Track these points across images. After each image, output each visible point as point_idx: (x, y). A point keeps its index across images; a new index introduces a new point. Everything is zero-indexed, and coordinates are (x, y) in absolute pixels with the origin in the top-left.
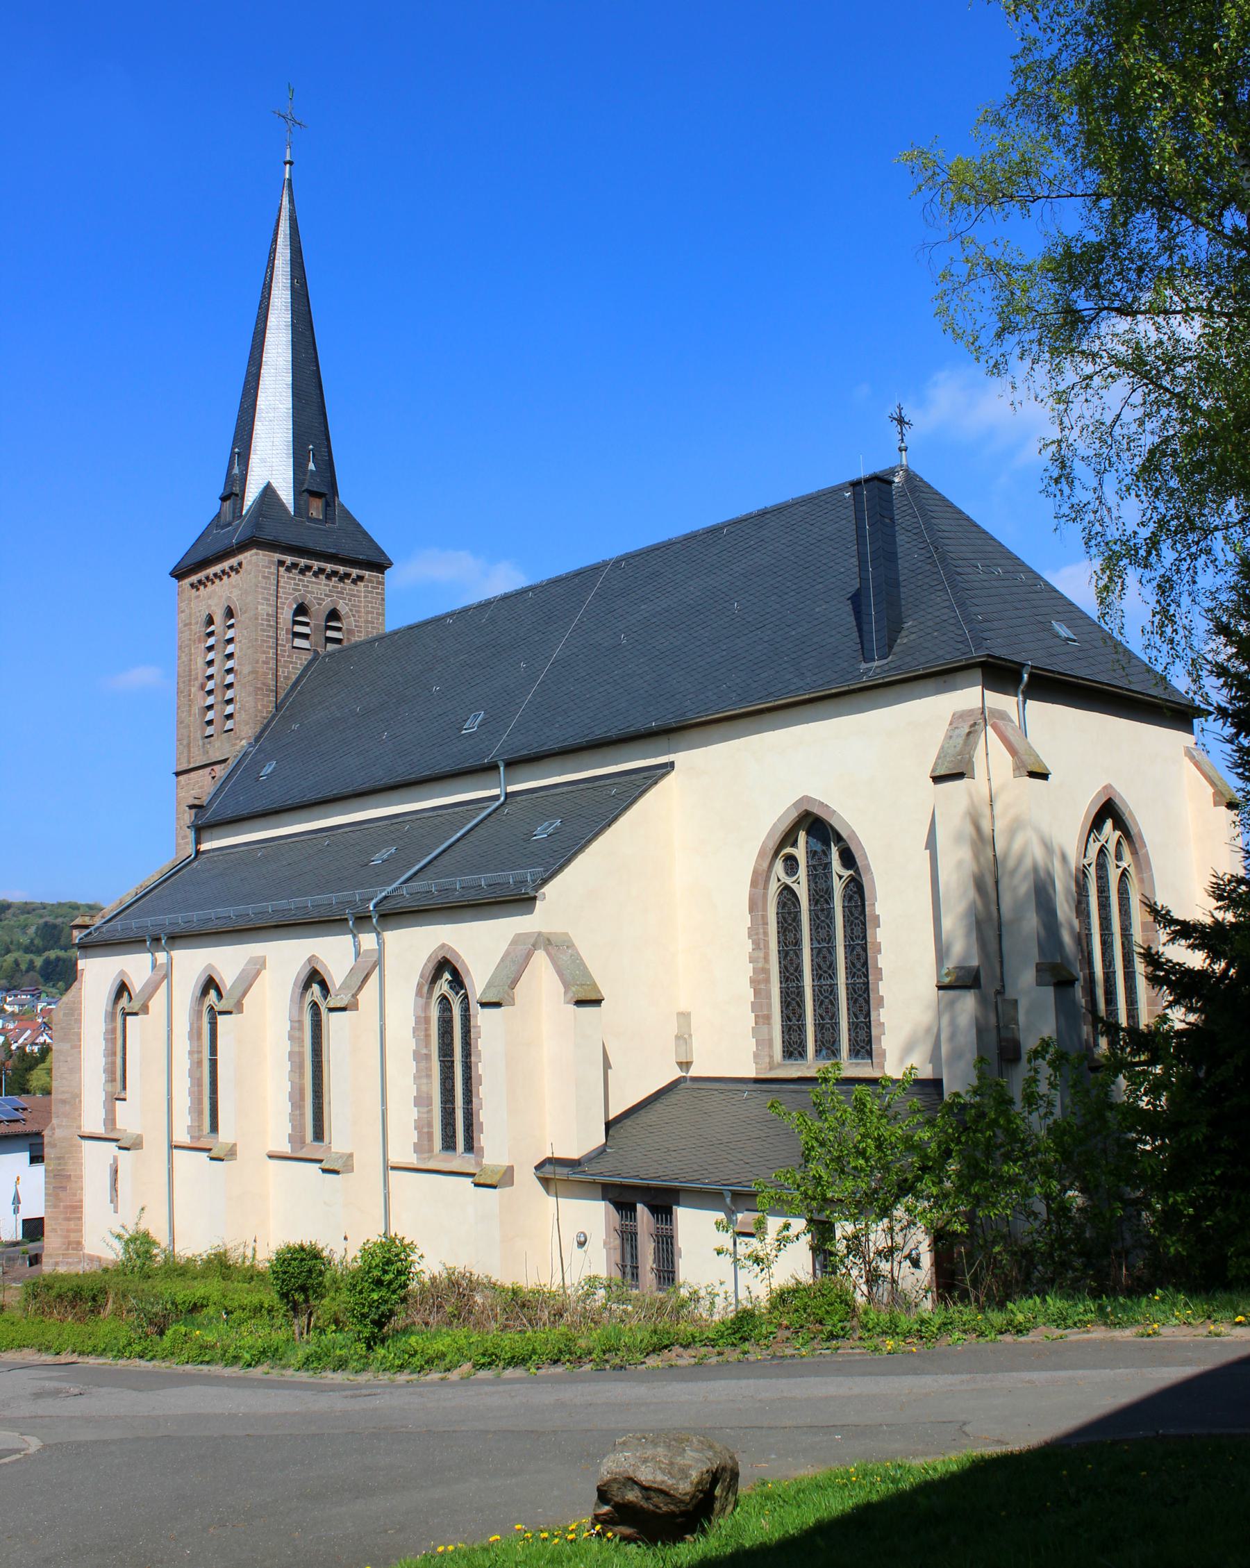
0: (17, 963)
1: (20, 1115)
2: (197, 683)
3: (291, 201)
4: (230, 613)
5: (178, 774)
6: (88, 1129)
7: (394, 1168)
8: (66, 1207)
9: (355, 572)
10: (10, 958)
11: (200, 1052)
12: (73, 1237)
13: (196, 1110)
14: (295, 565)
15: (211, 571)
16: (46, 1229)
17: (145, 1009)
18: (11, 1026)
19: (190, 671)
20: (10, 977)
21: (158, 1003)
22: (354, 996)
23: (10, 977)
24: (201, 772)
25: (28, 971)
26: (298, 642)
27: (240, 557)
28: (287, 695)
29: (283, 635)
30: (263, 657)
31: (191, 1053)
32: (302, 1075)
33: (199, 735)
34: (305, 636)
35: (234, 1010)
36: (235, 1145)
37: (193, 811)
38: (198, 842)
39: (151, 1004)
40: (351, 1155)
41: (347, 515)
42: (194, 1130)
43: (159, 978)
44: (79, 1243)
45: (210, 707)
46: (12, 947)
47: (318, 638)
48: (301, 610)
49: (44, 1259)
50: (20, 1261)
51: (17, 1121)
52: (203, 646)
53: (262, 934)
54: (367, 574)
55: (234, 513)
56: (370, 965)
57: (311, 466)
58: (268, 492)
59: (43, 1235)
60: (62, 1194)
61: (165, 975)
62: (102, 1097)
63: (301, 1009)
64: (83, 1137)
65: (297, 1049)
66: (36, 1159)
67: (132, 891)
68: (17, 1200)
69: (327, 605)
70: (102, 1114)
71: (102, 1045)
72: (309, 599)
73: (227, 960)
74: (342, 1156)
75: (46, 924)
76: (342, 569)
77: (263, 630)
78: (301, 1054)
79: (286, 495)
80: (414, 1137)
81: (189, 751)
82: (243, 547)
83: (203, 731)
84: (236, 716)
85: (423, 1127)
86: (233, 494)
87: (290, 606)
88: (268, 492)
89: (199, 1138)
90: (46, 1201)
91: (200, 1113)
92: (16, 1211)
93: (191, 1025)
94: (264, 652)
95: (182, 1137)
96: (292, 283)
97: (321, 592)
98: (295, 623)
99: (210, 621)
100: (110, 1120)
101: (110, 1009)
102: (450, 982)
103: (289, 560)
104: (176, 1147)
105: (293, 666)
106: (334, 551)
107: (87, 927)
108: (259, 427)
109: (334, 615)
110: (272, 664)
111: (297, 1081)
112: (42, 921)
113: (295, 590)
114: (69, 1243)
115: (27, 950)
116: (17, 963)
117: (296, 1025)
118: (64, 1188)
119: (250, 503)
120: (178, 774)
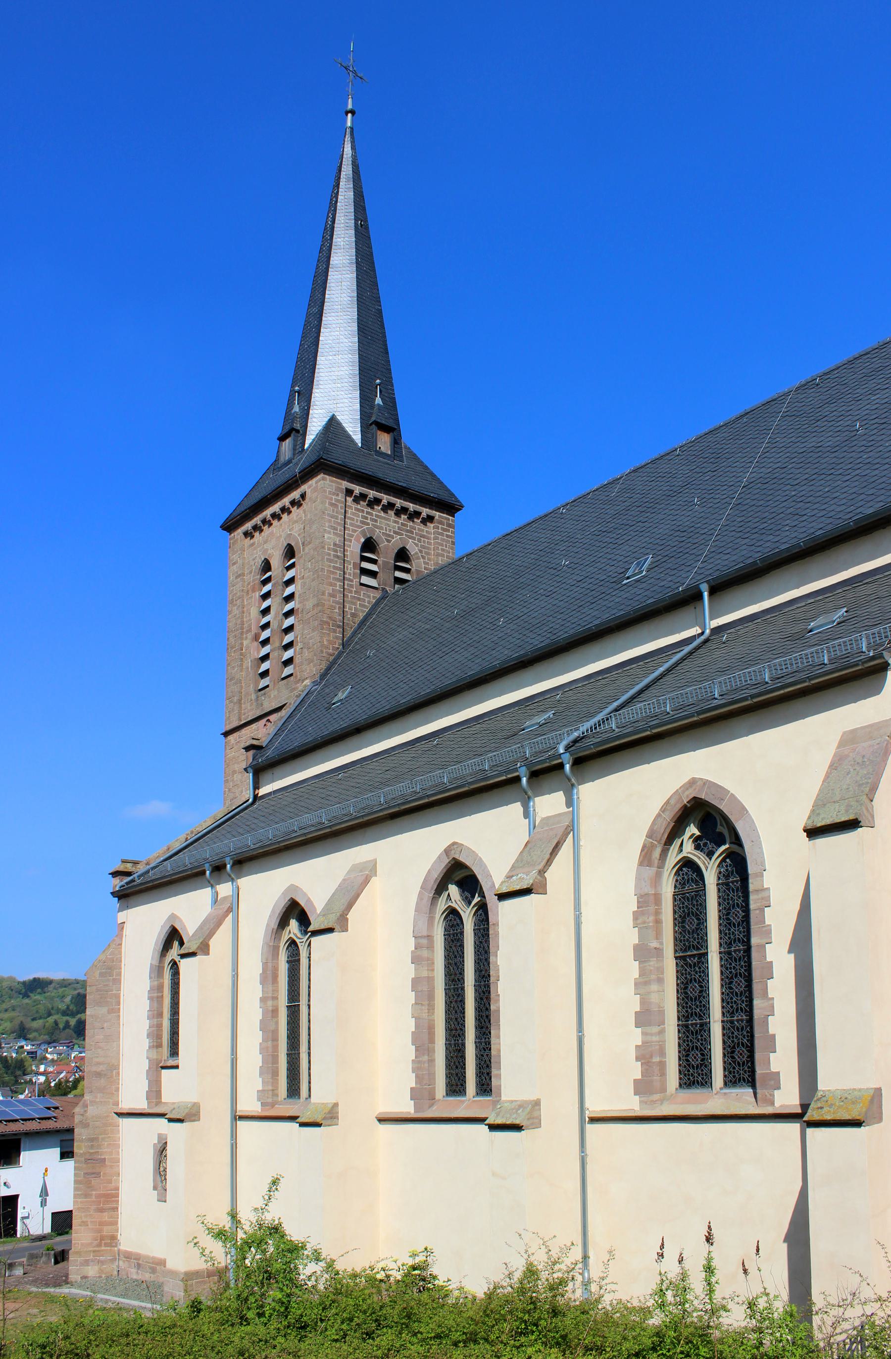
0: (56, 1023)
1: (51, 1113)
2: (250, 636)
3: (353, 142)
4: (290, 552)
5: (226, 734)
6: (126, 1105)
7: (593, 1120)
8: (99, 1196)
9: (425, 511)
10: (51, 1020)
11: (275, 998)
12: (107, 1231)
13: (269, 1069)
14: (363, 496)
15: (267, 513)
16: (75, 1222)
17: (204, 948)
18: (51, 1069)
19: (242, 623)
20: (51, 1034)
21: (220, 942)
22: (542, 872)
23: (51, 1034)
24: (254, 726)
25: (64, 1028)
26: (365, 580)
27: (304, 488)
28: (355, 633)
29: (350, 570)
30: (330, 589)
31: (263, 1000)
32: (431, 1008)
33: (252, 688)
34: (373, 574)
35: (337, 927)
36: (336, 1105)
37: (251, 753)
38: (256, 786)
39: (212, 943)
40: (537, 1103)
41: (414, 457)
42: (266, 1096)
43: (221, 912)
44: (114, 1238)
45: (265, 658)
46: (53, 1012)
47: (386, 577)
48: (369, 545)
49: (72, 1257)
50: (44, 1259)
51: (49, 1118)
52: (257, 595)
53: (370, 831)
54: (437, 514)
55: (294, 449)
56: (560, 832)
57: (378, 401)
58: (333, 425)
59: (71, 1227)
60: (94, 1182)
61: (230, 909)
62: (146, 1065)
63: (431, 919)
64: (120, 1115)
65: (425, 974)
66: (66, 1154)
67: (182, 837)
68: (44, 1192)
69: (396, 543)
70: (144, 1086)
71: (145, 1005)
72: (378, 535)
73: (315, 878)
74: (522, 1105)
75: (79, 994)
76: (412, 507)
77: (330, 561)
78: (430, 980)
79: (353, 429)
80: (636, 1071)
81: (241, 707)
82: (307, 474)
83: (257, 684)
84: (297, 660)
85: (647, 1056)
86: (293, 430)
87: (358, 540)
88: (333, 425)
89: (273, 1105)
90: (76, 1189)
91: (275, 1073)
92: (44, 1203)
93: (265, 965)
94: (331, 584)
95: (249, 1104)
96: (356, 224)
97: (389, 529)
98: (364, 559)
99: (267, 566)
100: (155, 1091)
101: (156, 962)
102: (695, 841)
103: (357, 489)
104: (242, 1118)
105: (361, 603)
106: (404, 485)
107: (128, 874)
108: (323, 361)
109: (402, 555)
110: (339, 597)
111: (425, 1015)
112: (76, 992)
113: (362, 522)
114: (102, 1238)
115: (65, 1013)
116: (56, 1023)
117: (423, 941)
118: (97, 1175)
119: (313, 437)
120: (226, 734)
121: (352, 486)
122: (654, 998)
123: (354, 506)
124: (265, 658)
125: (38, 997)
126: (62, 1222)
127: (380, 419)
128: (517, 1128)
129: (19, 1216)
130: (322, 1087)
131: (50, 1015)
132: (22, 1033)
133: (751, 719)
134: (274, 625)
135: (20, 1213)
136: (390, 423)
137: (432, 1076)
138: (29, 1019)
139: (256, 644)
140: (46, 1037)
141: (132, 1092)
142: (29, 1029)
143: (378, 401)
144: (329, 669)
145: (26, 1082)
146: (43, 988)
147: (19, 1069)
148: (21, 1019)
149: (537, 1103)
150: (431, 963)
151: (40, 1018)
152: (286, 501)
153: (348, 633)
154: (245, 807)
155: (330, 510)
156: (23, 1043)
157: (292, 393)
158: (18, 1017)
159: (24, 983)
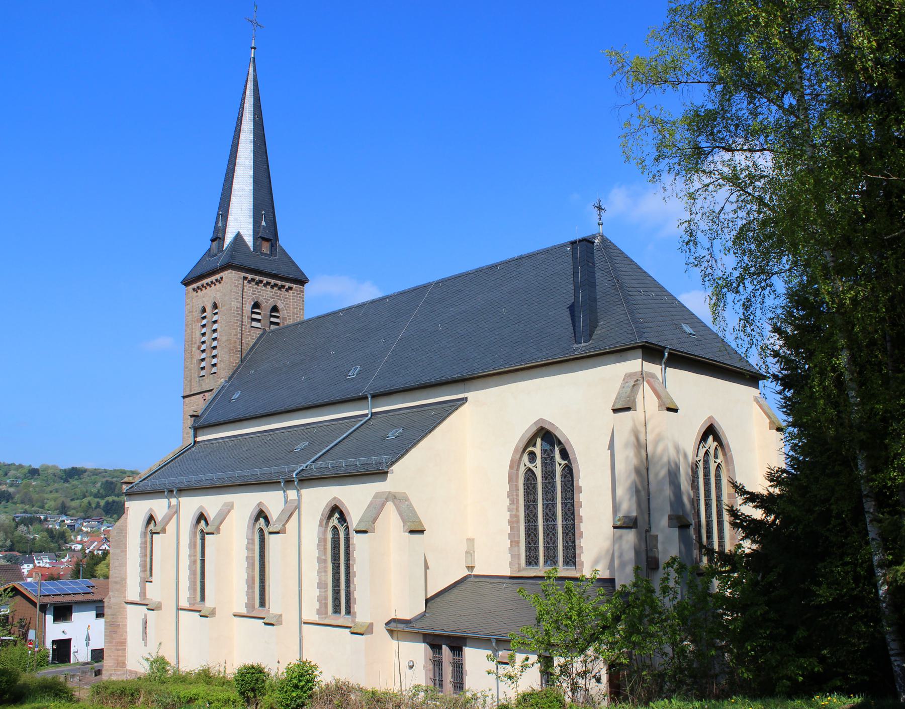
0: (89, 503)
1: (91, 590)
2: (196, 346)
3: (255, 70)
4: (215, 306)
5: (184, 397)
6: (130, 598)
7: (305, 623)
9: (287, 285)
10: (86, 500)
13: (192, 588)
14: (253, 280)
15: (205, 282)
17: (164, 531)
18: (86, 539)
20: (86, 511)
21: (171, 527)
22: (284, 525)
23: (86, 511)
26: (254, 324)
27: (222, 274)
29: (246, 320)
32: (253, 569)
33: (196, 375)
34: (258, 321)
38: (195, 436)
40: (281, 615)
41: (284, 252)
42: (191, 600)
44: (124, 663)
45: (203, 360)
48: (256, 305)
52: (200, 325)
54: (294, 286)
57: (263, 223)
58: (238, 237)
63: (253, 532)
64: (127, 603)
66: (99, 615)
67: (157, 463)
68: (88, 639)
72: (261, 300)
75: (107, 481)
76: (280, 283)
78: (253, 558)
79: (249, 239)
82: (223, 268)
83: (199, 373)
85: (322, 600)
86: (218, 237)
88: (238, 237)
89: (194, 604)
92: (88, 645)
95: (184, 603)
97: (267, 295)
98: (253, 313)
99: (204, 310)
100: (143, 593)
103: (250, 276)
105: (251, 337)
107: (131, 483)
108: (234, 200)
109: (275, 309)
110: (239, 336)
112: (104, 480)
114: (118, 663)
115: (96, 496)
117: (251, 541)
120: (184, 397)
121: (246, 275)
122: (323, 578)
123: (248, 285)
124: (203, 360)
125: (75, 482)
126: (98, 655)
127: (267, 232)
128: (272, 625)
129: (72, 650)
130: (209, 603)
131: (85, 497)
132: (64, 510)
133: (351, 479)
134: (208, 343)
135: (73, 649)
136: (270, 237)
137: (253, 599)
138: (69, 499)
139: (199, 351)
140: (82, 514)
141: (133, 594)
142: (69, 508)
143: (263, 223)
144: (233, 374)
145: (67, 549)
146: (79, 475)
147: (62, 538)
148: (63, 499)
149: (281, 615)
150: (253, 550)
151: (78, 499)
152: (213, 278)
153: (244, 354)
154: (188, 448)
155: (235, 289)
156: (64, 518)
157: (218, 215)
158: (61, 498)
159: (65, 471)
